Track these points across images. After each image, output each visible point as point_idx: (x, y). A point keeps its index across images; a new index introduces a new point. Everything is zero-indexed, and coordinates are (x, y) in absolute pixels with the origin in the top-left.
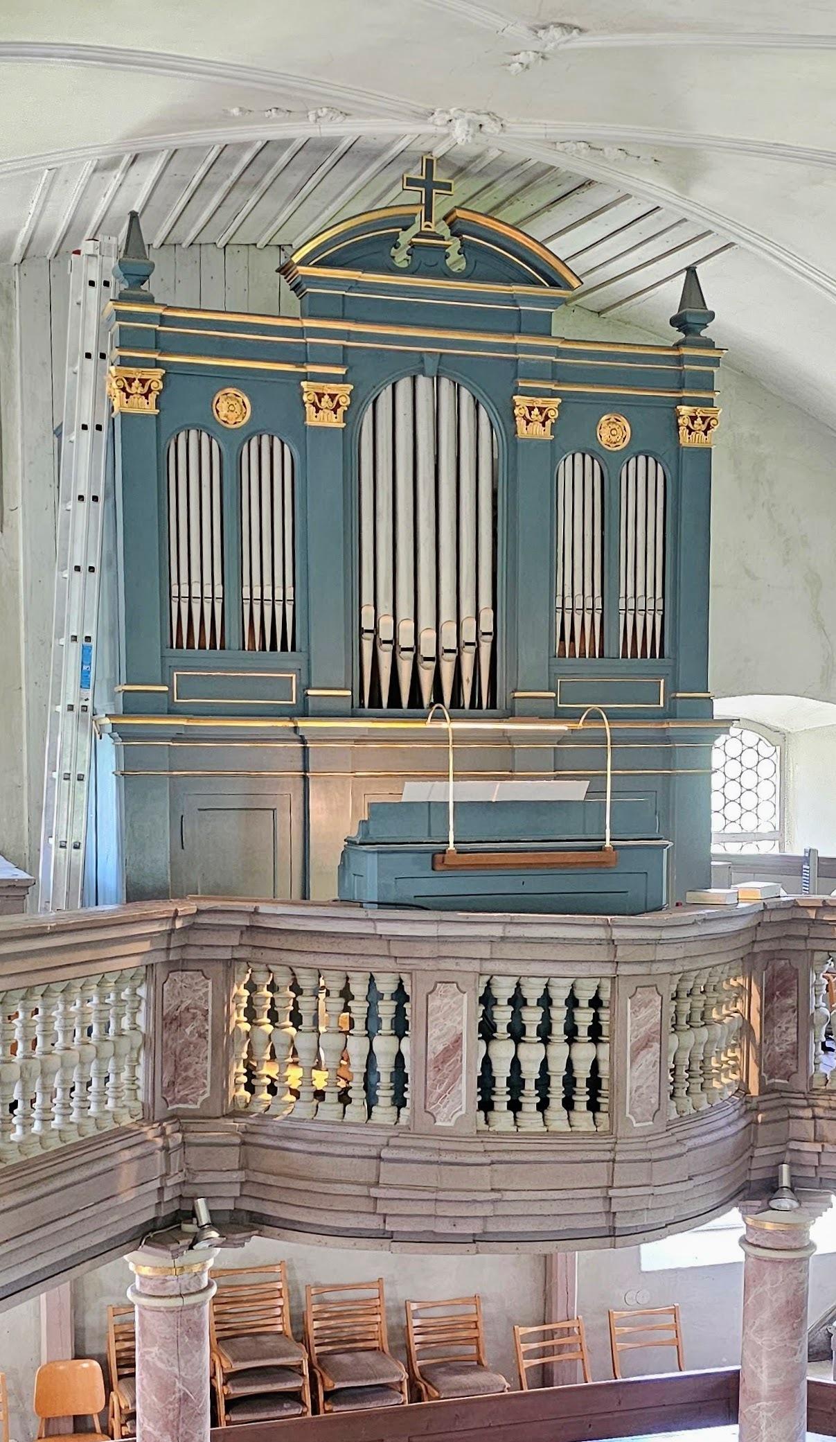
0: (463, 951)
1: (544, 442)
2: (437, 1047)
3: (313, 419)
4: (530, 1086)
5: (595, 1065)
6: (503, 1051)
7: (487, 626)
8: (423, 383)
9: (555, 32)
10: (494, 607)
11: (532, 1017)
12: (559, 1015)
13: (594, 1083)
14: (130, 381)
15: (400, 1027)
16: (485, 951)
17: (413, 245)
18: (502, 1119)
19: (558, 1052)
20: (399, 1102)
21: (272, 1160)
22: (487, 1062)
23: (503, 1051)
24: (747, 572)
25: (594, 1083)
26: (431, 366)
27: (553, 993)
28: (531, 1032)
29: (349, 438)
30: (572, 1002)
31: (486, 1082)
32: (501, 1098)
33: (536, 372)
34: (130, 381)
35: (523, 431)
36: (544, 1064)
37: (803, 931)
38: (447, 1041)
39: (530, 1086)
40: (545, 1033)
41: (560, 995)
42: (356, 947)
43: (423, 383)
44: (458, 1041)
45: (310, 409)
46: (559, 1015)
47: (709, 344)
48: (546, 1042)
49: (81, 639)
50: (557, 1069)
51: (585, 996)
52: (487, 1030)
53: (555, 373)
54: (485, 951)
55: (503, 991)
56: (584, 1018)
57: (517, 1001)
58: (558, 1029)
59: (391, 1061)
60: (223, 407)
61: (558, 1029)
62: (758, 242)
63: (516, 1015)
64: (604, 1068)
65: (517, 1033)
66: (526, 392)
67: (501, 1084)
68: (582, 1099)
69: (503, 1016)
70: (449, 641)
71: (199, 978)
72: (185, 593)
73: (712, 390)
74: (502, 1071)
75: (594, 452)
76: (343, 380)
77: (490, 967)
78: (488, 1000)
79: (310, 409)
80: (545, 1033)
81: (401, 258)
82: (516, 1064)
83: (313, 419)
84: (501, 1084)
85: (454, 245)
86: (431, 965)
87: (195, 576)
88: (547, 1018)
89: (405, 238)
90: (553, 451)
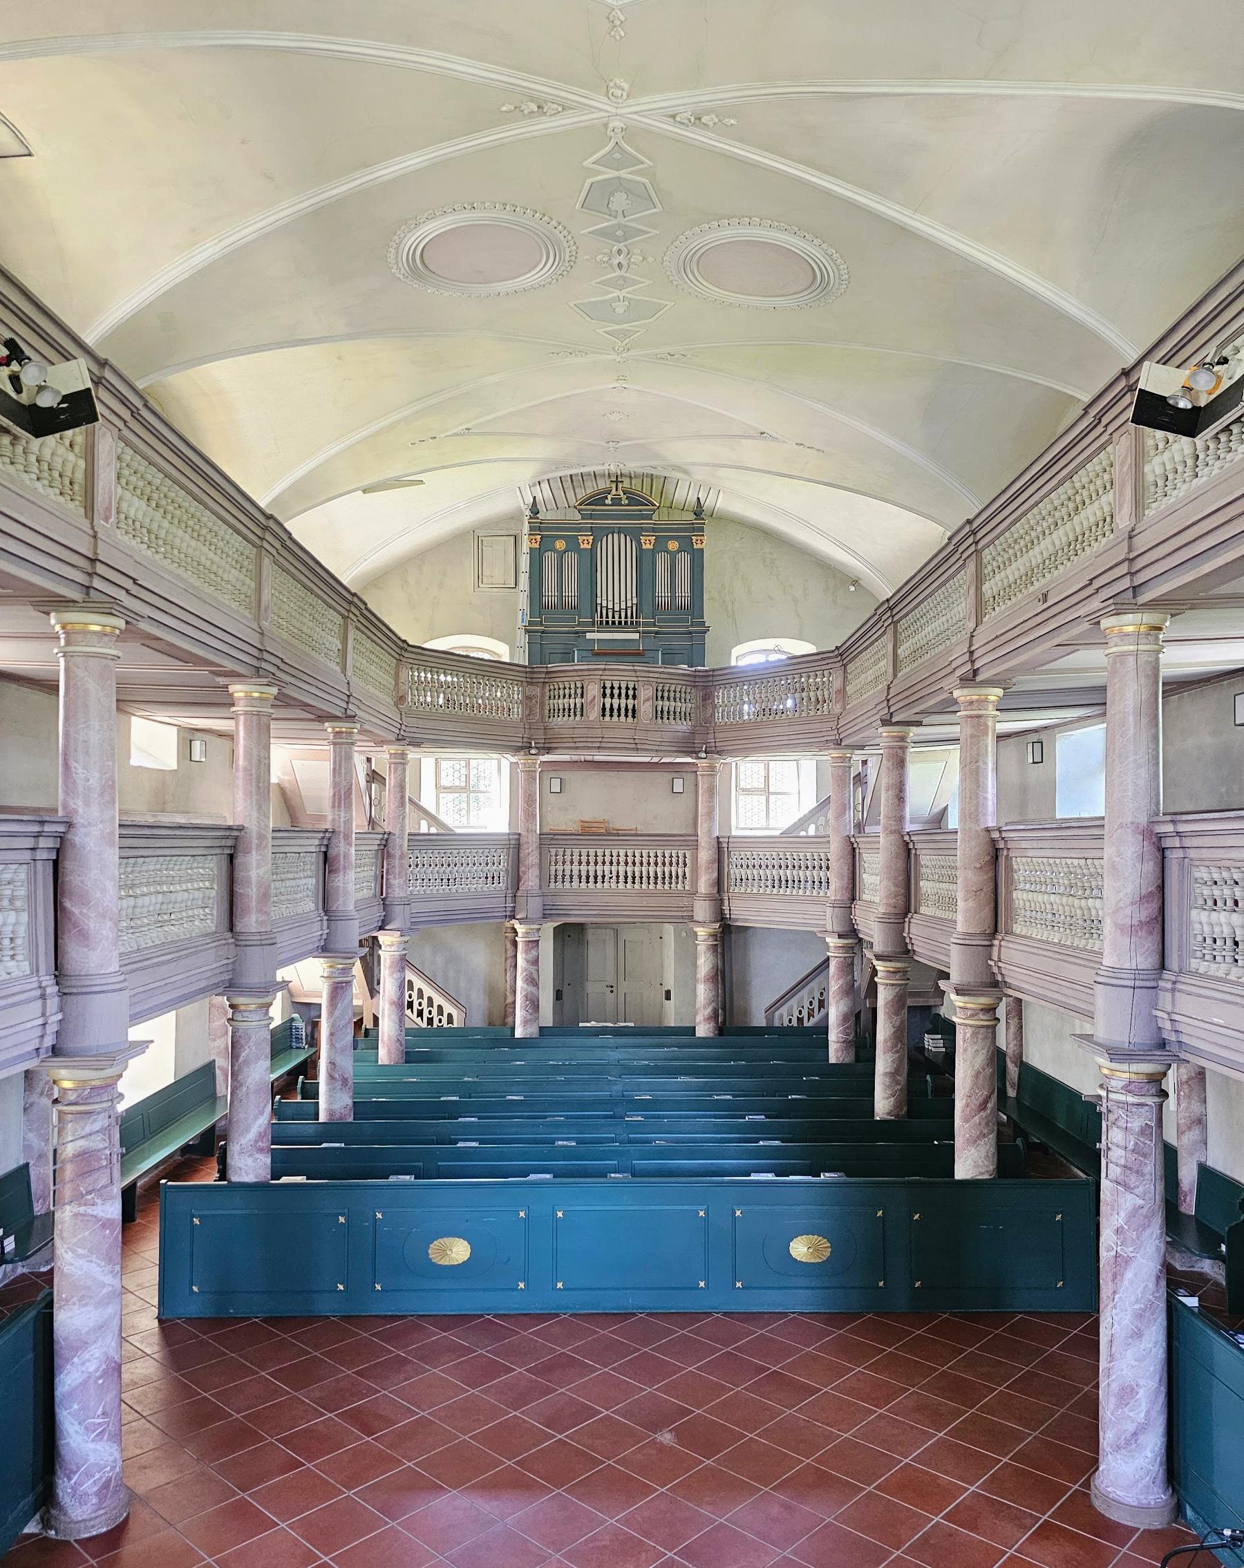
0: (596, 673)
2: (589, 699)
3: (582, 546)
6: (608, 701)
7: (635, 602)
8: (616, 535)
11: (616, 692)
12: (623, 691)
13: (634, 710)
16: (601, 673)
18: (607, 718)
19: (623, 701)
20: (582, 715)
21: (551, 732)
22: (604, 704)
23: (608, 701)
25: (634, 710)
26: (616, 530)
28: (616, 696)
29: (593, 551)
30: (627, 688)
31: (604, 709)
32: (608, 713)
33: (647, 530)
35: (644, 547)
37: (711, 679)
41: (623, 686)
42: (570, 674)
43: (616, 535)
46: (623, 691)
50: (623, 706)
51: (631, 686)
52: (604, 696)
53: (654, 530)
54: (601, 673)
55: (608, 685)
56: (631, 692)
57: (612, 688)
58: (623, 695)
61: (623, 695)
63: (612, 692)
65: (612, 696)
67: (608, 710)
68: (630, 714)
69: (608, 691)
70: (623, 606)
74: (608, 706)
75: (668, 552)
77: (603, 678)
78: (604, 688)
81: (608, 501)
82: (612, 705)
83: (582, 546)
84: (608, 710)
88: (620, 693)
89: (609, 497)
90: (653, 552)
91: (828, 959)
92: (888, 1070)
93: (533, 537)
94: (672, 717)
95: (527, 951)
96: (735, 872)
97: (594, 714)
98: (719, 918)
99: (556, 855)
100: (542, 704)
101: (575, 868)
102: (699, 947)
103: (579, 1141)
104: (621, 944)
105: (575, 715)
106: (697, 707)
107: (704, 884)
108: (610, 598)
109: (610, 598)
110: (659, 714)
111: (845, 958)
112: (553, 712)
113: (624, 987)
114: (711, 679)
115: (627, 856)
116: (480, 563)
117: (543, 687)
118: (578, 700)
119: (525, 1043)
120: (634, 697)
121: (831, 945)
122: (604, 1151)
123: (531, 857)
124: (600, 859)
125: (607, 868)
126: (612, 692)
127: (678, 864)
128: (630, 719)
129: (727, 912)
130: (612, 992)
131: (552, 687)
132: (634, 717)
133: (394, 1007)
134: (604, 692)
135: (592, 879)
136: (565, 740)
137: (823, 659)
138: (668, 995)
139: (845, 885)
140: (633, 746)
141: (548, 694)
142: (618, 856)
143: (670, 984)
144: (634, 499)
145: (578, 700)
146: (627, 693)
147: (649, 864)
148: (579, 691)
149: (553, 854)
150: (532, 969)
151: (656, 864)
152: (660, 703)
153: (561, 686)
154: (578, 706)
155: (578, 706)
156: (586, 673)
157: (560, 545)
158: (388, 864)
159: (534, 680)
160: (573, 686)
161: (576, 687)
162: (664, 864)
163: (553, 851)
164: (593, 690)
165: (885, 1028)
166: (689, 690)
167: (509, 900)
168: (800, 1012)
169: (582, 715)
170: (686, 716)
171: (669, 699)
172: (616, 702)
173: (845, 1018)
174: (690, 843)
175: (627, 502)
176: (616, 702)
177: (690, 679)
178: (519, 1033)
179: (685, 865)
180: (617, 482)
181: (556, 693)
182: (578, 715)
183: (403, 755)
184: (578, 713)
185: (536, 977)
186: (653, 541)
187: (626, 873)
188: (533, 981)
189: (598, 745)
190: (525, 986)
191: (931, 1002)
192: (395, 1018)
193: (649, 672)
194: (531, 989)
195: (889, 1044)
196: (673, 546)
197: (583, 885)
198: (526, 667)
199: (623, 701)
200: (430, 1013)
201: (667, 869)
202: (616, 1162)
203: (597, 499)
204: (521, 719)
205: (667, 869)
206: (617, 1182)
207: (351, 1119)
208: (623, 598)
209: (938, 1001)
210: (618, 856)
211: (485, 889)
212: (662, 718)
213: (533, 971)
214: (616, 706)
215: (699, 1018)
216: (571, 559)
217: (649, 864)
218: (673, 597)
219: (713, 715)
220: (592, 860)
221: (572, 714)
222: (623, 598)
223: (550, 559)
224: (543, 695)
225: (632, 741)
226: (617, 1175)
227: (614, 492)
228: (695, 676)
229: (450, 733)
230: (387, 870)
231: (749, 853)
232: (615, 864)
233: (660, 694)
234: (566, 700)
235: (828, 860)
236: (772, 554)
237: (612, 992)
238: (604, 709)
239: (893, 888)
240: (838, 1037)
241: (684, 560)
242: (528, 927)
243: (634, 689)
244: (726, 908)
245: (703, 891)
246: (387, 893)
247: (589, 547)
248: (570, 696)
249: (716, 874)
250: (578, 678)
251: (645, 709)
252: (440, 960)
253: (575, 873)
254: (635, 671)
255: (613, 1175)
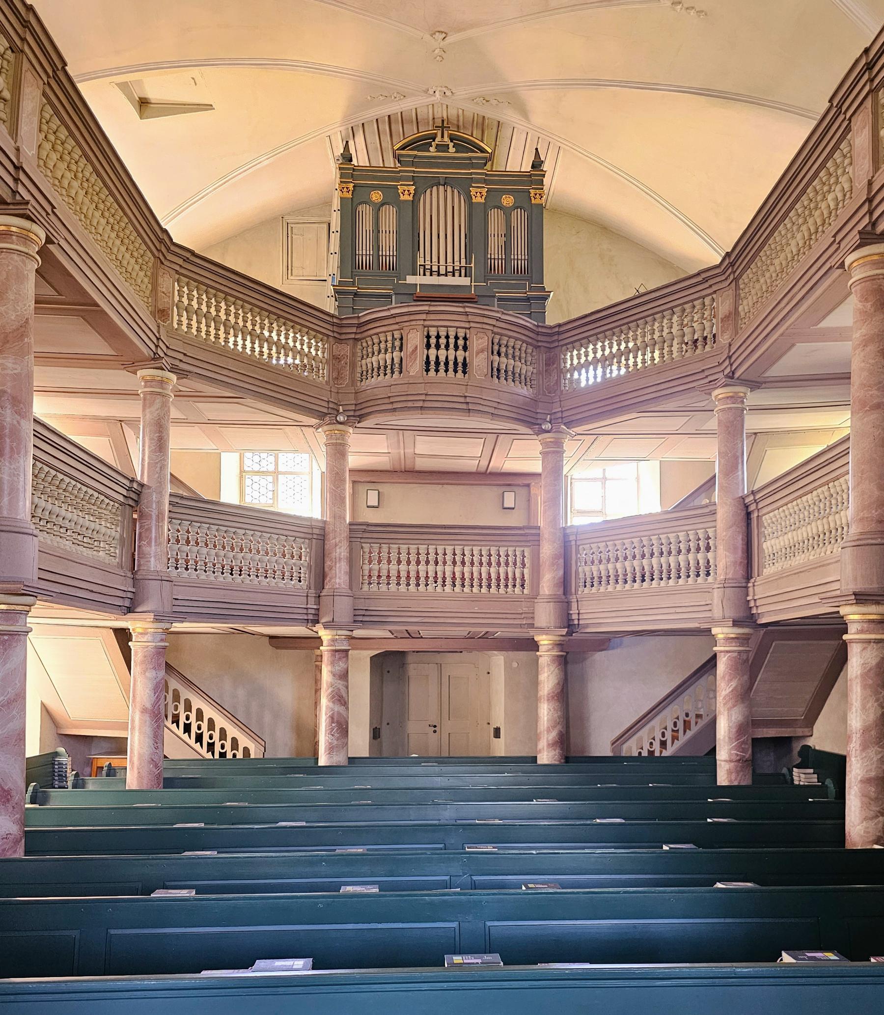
1: (480, 203)
2: (410, 350)
3: (402, 198)
4: (442, 364)
5: (465, 359)
6: (433, 352)
8: (441, 188)
9: (437, 34)
10: (466, 258)
11: (443, 341)
12: (452, 341)
14: (343, 188)
15: (401, 350)
17: (437, 145)
18: (432, 373)
19: (452, 352)
21: (363, 395)
23: (433, 352)
24: (608, 297)
25: (465, 364)
27: (450, 333)
28: (443, 346)
29: (414, 203)
30: (457, 338)
31: (428, 362)
34: (343, 188)
35: (474, 200)
36: (447, 358)
38: (413, 348)
39: (442, 364)
40: (447, 347)
41: (452, 334)
44: (416, 347)
45: (402, 195)
46: (452, 341)
47: (542, 170)
48: (447, 350)
49: (332, 275)
51: (461, 334)
52: (428, 346)
53: (485, 182)
54: (424, 316)
55: (433, 332)
56: (461, 342)
58: (452, 346)
59: (453, 358)
60: (374, 196)
61: (452, 346)
62: (564, 142)
63: (438, 342)
64: (467, 359)
65: (438, 347)
66: (473, 187)
67: (432, 363)
68: (460, 368)
69: (433, 341)
71: (346, 345)
72: (361, 253)
73: (543, 185)
74: (433, 358)
75: (500, 207)
76: (412, 185)
77: (427, 323)
78: (428, 337)
79: (402, 195)
80: (447, 347)
82: (437, 357)
83: (402, 198)
84: (432, 363)
85: (451, 145)
86: (407, 324)
87: (364, 248)
88: (448, 342)
91: (714, 657)
92: (873, 774)
93: (344, 185)
94: (510, 378)
95: (333, 663)
96: (585, 570)
97: (415, 368)
98: (566, 625)
99: (370, 553)
100: (353, 366)
101: (393, 567)
102: (541, 660)
103: (383, 887)
104: (445, 680)
105: (393, 373)
106: (539, 373)
107: (548, 584)
108: (435, 259)
109: (435, 259)
110: (496, 372)
111: (739, 652)
112: (364, 376)
113: (448, 726)
114: (556, 337)
115: (454, 554)
116: (289, 252)
117: (355, 346)
118: (396, 354)
119: (328, 770)
120: (465, 348)
121: (720, 636)
122: (431, 903)
123: (340, 551)
124: (423, 558)
125: (431, 568)
126: (438, 342)
127: (515, 564)
128: (460, 374)
129: (575, 617)
130: (435, 732)
131: (364, 344)
132: (464, 372)
133: (147, 718)
134: (428, 342)
135: (413, 581)
136: (379, 402)
137: (705, 280)
138: (497, 733)
139: (739, 560)
140: (464, 406)
141: (360, 354)
142: (445, 554)
143: (499, 719)
144: (462, 144)
145: (396, 354)
146: (456, 343)
147: (481, 564)
148: (397, 343)
149: (367, 550)
150: (340, 684)
151: (489, 564)
152: (496, 358)
153: (376, 341)
154: (396, 360)
155: (396, 360)
156: (406, 318)
157: (377, 196)
158: (141, 527)
159: (343, 337)
160: (390, 338)
161: (394, 339)
162: (499, 564)
163: (366, 547)
164: (415, 339)
165: (864, 707)
166: (530, 351)
167: (312, 600)
168: (663, 735)
169: (401, 372)
170: (526, 381)
171: (506, 355)
172: (442, 353)
173: (741, 730)
174: (529, 538)
175: (454, 150)
176: (442, 353)
177: (531, 335)
178: (323, 761)
179: (524, 565)
180: (443, 127)
181: (370, 350)
182: (396, 373)
183: (162, 382)
184: (396, 370)
185: (344, 695)
186: (485, 194)
187: (454, 573)
188: (341, 699)
189: (420, 404)
190: (331, 705)
191: (799, 732)
192: (148, 730)
193: (484, 316)
194: (337, 708)
195: (873, 733)
196: (508, 201)
197: (403, 588)
198: (333, 316)
199: (452, 352)
200: (223, 747)
201: (502, 570)
202: (455, 925)
203: (422, 143)
204: (327, 383)
205: (502, 570)
206: (469, 977)
207: (20, 854)
208: (450, 259)
209: (806, 731)
210: (445, 554)
211: (281, 585)
212: (498, 377)
213: (341, 687)
214: (442, 359)
215: (543, 743)
216: (389, 216)
217: (481, 564)
218: (508, 259)
219: (558, 382)
220: (413, 558)
221: (389, 371)
222: (450, 259)
223: (366, 213)
224: (354, 354)
225: (462, 400)
226: (469, 959)
227: (438, 139)
228: (538, 334)
229: (231, 374)
230: (140, 534)
231: (602, 545)
232: (440, 563)
233: (496, 348)
234: (381, 356)
235: (709, 538)
236: (610, 251)
237: (435, 732)
238: (428, 362)
239: (877, 493)
240: (730, 754)
241: (518, 219)
242: (334, 632)
243: (465, 339)
244: (574, 611)
245: (547, 592)
246: (139, 565)
247: (411, 198)
248: (386, 350)
249: (561, 572)
250: (396, 327)
251: (479, 362)
252: (241, 692)
253: (394, 573)
254: (466, 314)
255: (458, 959)
